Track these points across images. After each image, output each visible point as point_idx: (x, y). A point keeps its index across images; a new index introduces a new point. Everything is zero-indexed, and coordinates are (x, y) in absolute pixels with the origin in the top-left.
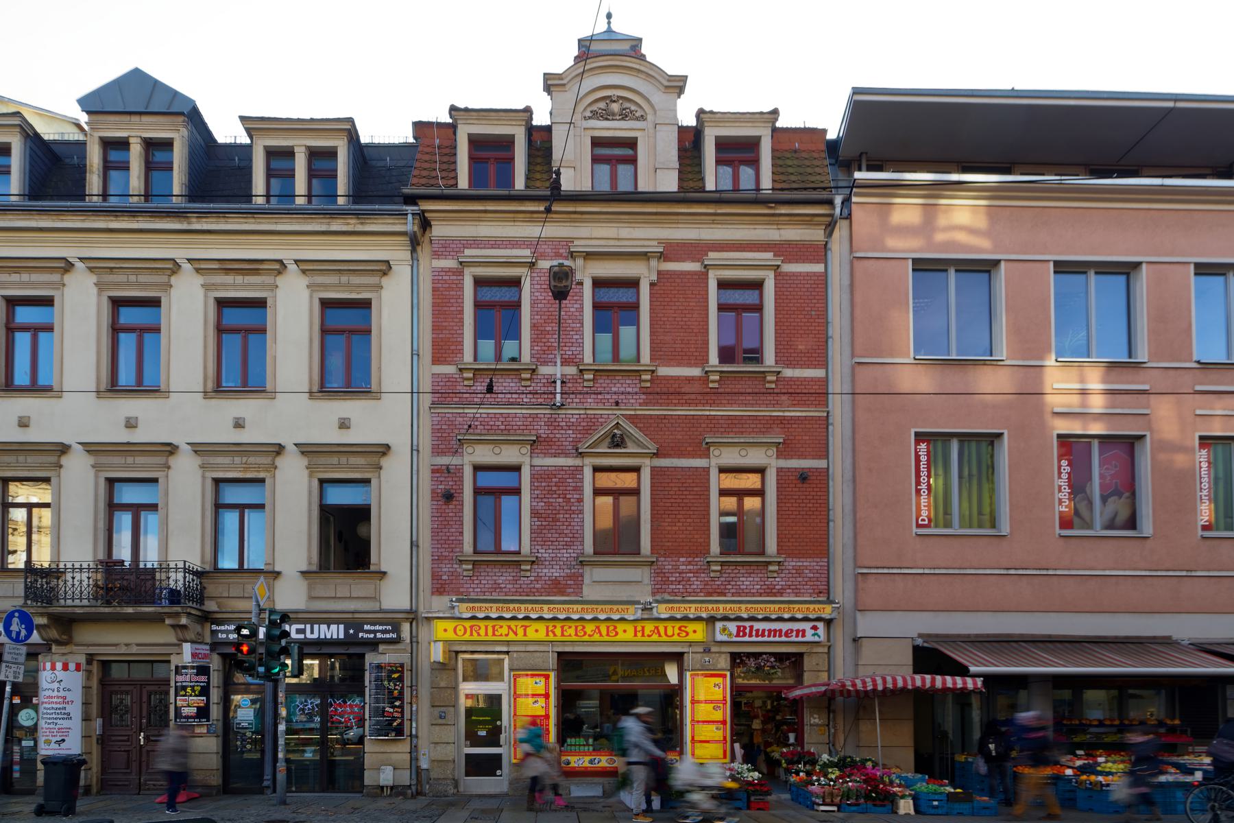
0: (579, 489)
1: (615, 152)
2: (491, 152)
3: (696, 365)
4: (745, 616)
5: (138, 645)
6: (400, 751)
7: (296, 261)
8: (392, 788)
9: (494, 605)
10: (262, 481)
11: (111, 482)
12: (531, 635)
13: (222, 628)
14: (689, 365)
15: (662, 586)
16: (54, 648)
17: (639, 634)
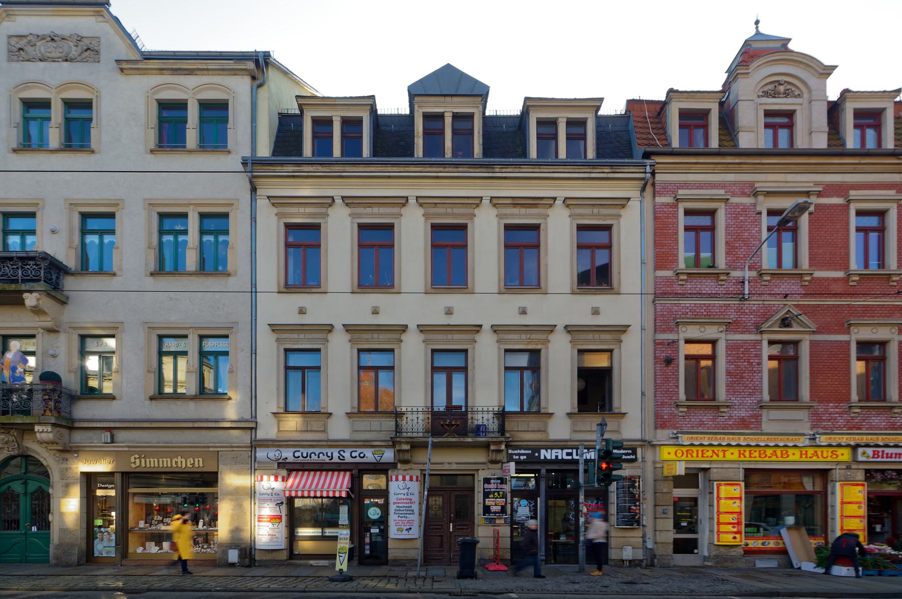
0: (759, 356)
1: (781, 120)
2: (694, 119)
3: (840, 270)
4: (881, 444)
5: (457, 463)
6: (635, 536)
7: (343, 197)
8: (630, 561)
9: (707, 436)
10: (319, 350)
11: (581, 352)
12: (729, 456)
13: (516, 452)
14: (836, 270)
15: (817, 421)
16: (399, 465)
17: (804, 456)
